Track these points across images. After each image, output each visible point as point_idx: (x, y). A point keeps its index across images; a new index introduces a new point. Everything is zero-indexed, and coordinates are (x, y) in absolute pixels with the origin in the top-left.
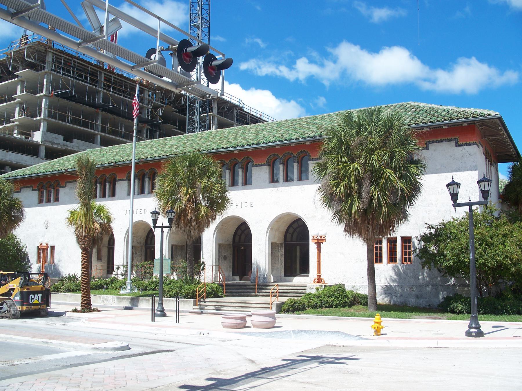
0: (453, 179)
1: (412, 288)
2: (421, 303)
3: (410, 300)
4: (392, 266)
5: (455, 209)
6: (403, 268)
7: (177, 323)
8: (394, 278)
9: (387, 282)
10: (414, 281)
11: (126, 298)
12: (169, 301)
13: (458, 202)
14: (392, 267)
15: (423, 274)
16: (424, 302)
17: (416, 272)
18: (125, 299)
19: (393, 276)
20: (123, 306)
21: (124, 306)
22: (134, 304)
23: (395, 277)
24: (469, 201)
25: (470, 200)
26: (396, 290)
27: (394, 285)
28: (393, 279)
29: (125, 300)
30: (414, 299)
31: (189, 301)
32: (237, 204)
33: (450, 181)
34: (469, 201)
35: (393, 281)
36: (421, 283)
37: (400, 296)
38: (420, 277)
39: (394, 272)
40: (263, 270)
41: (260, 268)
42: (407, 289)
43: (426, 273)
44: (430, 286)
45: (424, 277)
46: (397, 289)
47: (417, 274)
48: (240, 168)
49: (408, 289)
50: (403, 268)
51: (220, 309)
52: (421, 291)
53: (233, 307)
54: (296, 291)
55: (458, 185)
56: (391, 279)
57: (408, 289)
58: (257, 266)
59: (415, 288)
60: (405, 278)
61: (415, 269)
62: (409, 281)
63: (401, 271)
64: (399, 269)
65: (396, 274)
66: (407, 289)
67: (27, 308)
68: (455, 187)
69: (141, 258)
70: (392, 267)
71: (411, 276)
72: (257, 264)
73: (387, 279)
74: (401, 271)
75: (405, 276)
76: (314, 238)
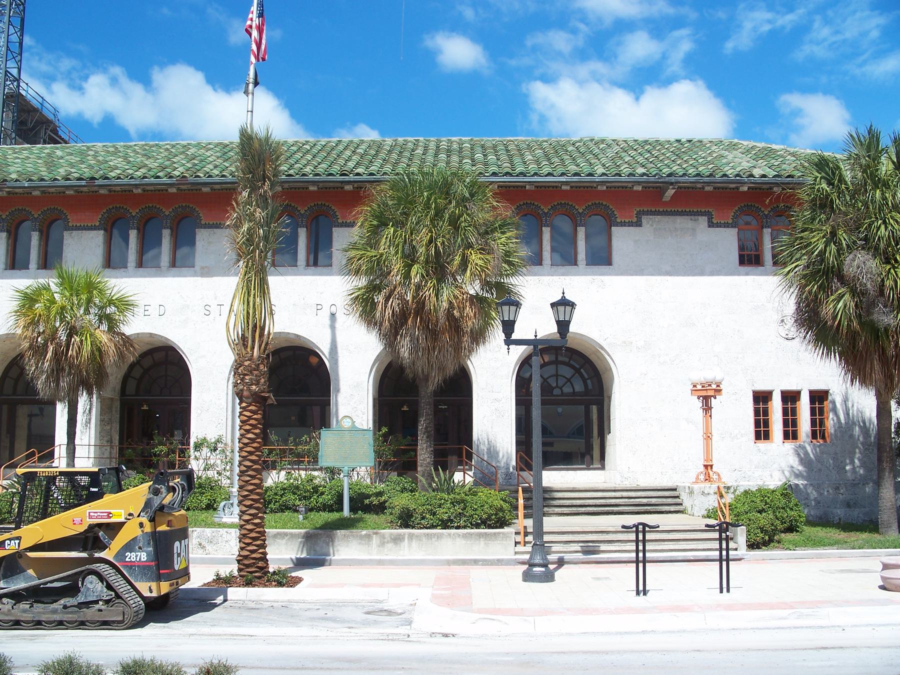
0: (563, 293)
1: (837, 488)
2: (856, 516)
3: (835, 511)
4: (793, 447)
5: (508, 349)
6: (816, 450)
7: (721, 592)
8: (798, 470)
9: (784, 478)
10: (837, 476)
11: (286, 534)
12: (439, 537)
13: (514, 336)
14: (794, 448)
15: (852, 462)
16: (861, 515)
17: (839, 458)
18: (283, 538)
19: (795, 466)
20: (288, 557)
21: (294, 557)
22: (318, 548)
23: (801, 468)
24: (534, 338)
25: (536, 336)
26: (808, 494)
27: (802, 484)
28: (797, 472)
29: (284, 541)
30: (843, 510)
31: (503, 533)
32: (147, 308)
33: (558, 297)
34: (534, 338)
35: (798, 475)
36: (850, 479)
37: (816, 505)
38: (848, 468)
39: (797, 459)
40: (505, 458)
41: (498, 453)
42: (828, 492)
43: (859, 460)
44: (871, 484)
45: (854, 468)
46: (809, 491)
47: (842, 462)
48: (36, 231)
49: (831, 491)
50: (816, 450)
51: (597, 549)
52: (855, 494)
53: (619, 544)
54: (626, 500)
55: (572, 305)
56: (793, 471)
57: (831, 491)
58: (489, 449)
59: (844, 489)
60: (820, 470)
61: (838, 452)
62: (827, 476)
63: (812, 456)
64: (806, 453)
65: (802, 461)
66: (826, 492)
67: (171, 585)
68: (568, 308)
69: (108, 428)
70: (794, 448)
71: (830, 465)
72: (489, 444)
73: (784, 473)
74: (812, 456)
75: (819, 466)
76: (695, 386)
